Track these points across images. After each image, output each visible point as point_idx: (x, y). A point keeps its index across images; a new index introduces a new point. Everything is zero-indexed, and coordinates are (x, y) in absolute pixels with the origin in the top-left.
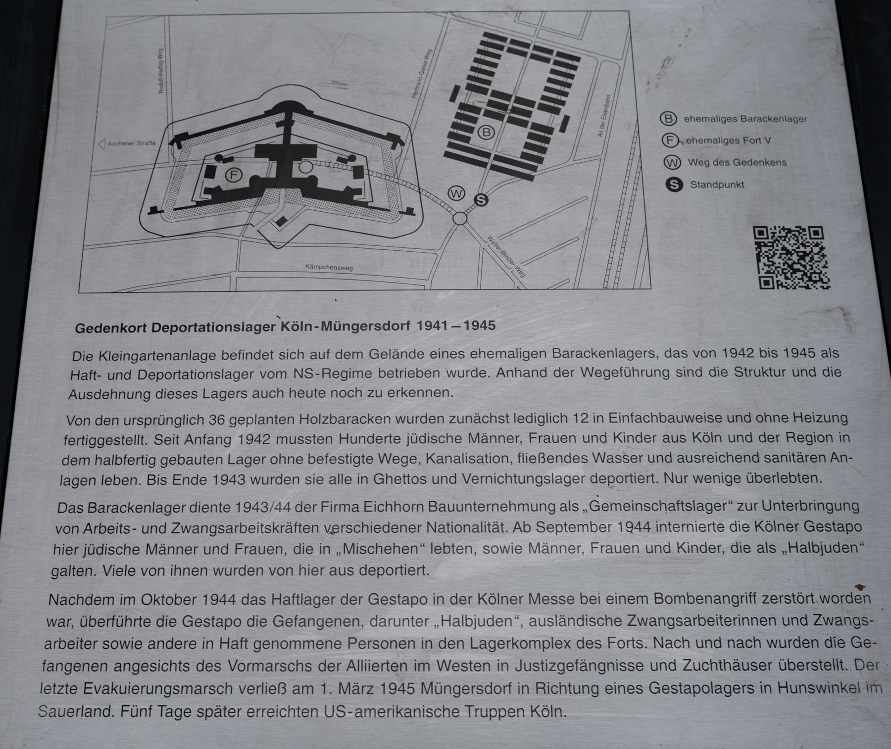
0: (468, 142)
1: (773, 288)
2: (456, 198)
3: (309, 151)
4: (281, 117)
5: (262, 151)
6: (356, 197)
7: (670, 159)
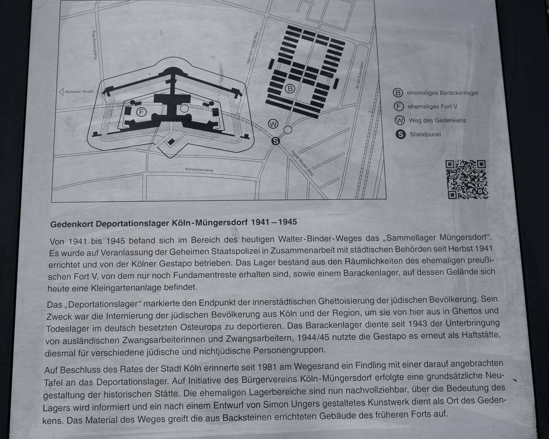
0: (279, 94)
1: (456, 198)
2: (273, 127)
3: (186, 99)
4: (169, 77)
5: (158, 98)
6: (214, 128)
7: (398, 118)
